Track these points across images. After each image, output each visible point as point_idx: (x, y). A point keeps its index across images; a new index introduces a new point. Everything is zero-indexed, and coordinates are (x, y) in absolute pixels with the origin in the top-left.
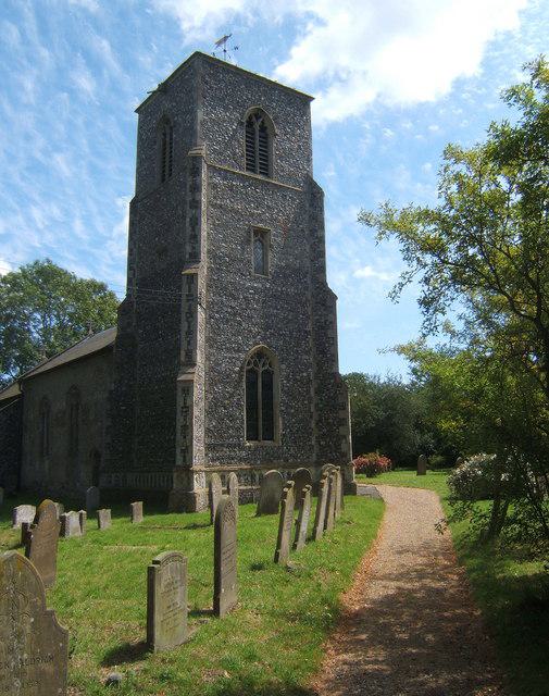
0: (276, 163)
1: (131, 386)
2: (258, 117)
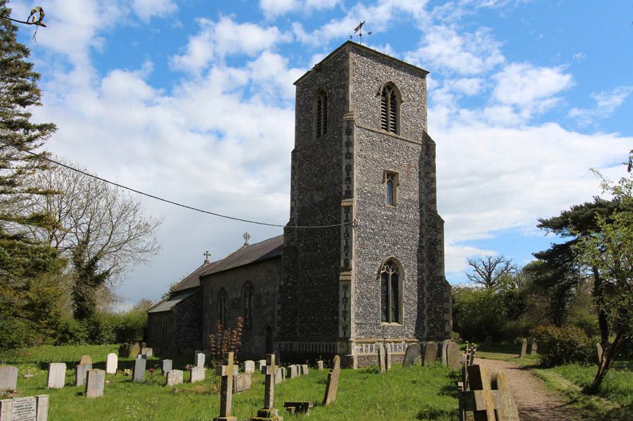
0: (402, 122)
1: (295, 283)
2: (389, 89)
